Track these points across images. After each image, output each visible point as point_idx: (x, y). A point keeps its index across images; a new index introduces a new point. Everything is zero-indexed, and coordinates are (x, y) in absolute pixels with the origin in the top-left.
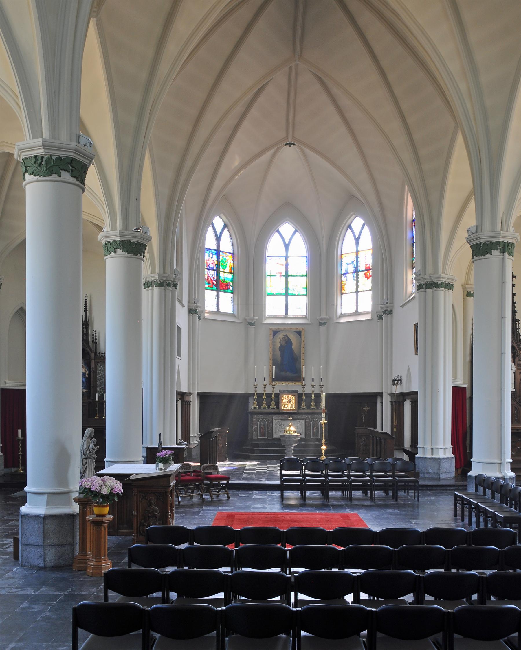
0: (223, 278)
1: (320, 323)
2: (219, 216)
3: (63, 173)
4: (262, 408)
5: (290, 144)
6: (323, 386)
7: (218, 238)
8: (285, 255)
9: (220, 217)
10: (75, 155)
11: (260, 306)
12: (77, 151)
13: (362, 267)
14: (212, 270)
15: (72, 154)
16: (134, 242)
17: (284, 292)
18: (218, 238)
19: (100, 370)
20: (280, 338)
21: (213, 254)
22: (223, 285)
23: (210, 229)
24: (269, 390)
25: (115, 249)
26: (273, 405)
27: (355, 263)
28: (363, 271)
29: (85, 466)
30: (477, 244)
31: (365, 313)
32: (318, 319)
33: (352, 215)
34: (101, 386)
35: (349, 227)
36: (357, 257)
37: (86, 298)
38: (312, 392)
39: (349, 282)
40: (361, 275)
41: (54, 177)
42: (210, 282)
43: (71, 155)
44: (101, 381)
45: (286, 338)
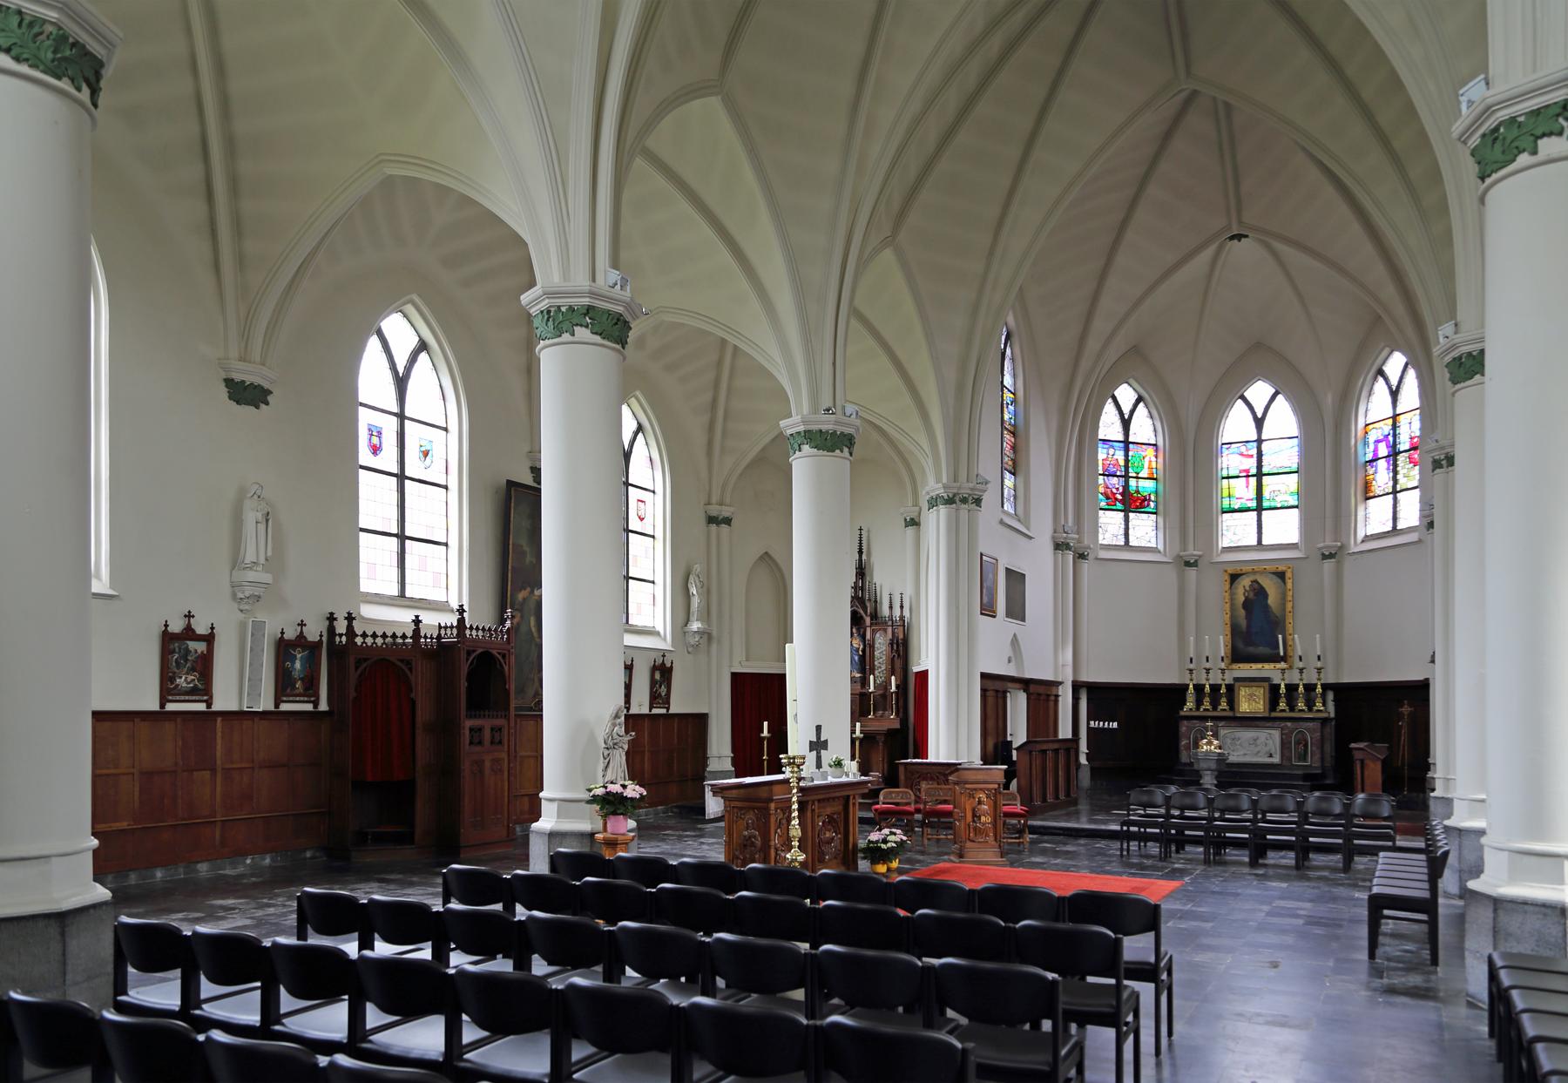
0: (1135, 488)
1: (1323, 554)
2: (1127, 383)
3: (577, 329)
4: (1202, 710)
5: (1239, 237)
7: (1126, 424)
8: (1255, 438)
9: (1129, 384)
10: (592, 301)
11: (1210, 530)
12: (592, 294)
13: (1404, 444)
14: (1114, 475)
15: (588, 299)
16: (827, 432)
17: (1253, 504)
18: (1126, 424)
19: (880, 643)
20: (1244, 587)
24: (1216, 678)
25: (799, 446)
26: (1224, 705)
27: (1391, 438)
28: (1405, 451)
29: (607, 760)
30: (1454, 359)
31: (1410, 530)
32: (1319, 549)
33: (1382, 350)
34: (880, 667)
35: (1381, 373)
36: (1394, 427)
38: (1297, 682)
39: (1381, 477)
40: (1401, 458)
41: (566, 337)
43: (586, 301)
45: (1256, 586)
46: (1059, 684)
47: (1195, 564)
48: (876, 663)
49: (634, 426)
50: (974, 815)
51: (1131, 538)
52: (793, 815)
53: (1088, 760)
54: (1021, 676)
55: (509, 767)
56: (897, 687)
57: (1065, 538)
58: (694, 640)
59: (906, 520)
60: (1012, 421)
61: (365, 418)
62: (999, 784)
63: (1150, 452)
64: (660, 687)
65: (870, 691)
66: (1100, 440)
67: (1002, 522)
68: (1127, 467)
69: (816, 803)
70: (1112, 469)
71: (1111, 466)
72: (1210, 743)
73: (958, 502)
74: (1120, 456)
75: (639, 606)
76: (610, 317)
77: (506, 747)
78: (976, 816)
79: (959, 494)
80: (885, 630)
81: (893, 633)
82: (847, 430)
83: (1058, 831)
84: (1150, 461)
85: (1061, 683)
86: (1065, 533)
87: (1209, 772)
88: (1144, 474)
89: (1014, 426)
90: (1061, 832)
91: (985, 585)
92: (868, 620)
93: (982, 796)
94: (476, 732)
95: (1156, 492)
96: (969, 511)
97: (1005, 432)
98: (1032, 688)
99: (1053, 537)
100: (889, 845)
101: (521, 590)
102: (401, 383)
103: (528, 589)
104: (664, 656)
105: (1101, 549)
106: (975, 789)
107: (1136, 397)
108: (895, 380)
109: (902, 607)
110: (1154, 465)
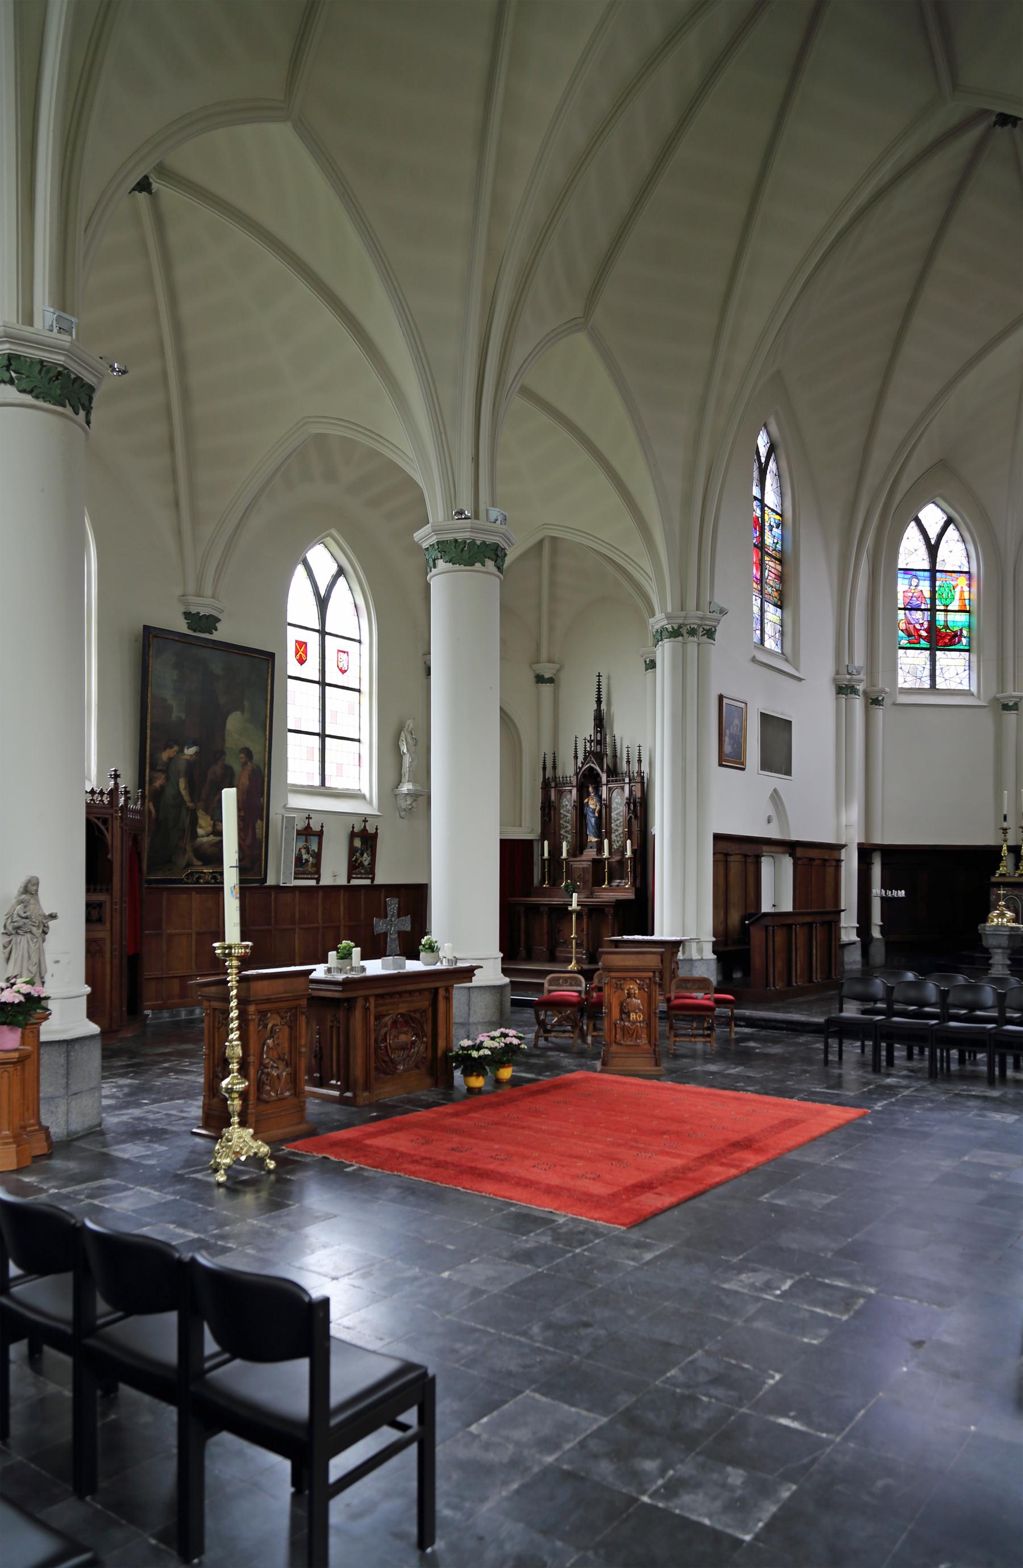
0: (942, 623)
2: (933, 503)
4: (997, 875)
6: (1008, 831)
7: (933, 550)
18: (933, 550)
19: (617, 803)
21: (919, 580)
22: (943, 636)
23: (912, 530)
25: (434, 560)
29: (8, 949)
37: (599, 679)
42: (912, 634)
44: (618, 822)
46: (841, 847)
47: (1015, 707)
48: (613, 825)
49: (334, 568)
50: (622, 1011)
51: (938, 680)
52: (231, 1026)
53: (882, 933)
54: (786, 838)
55: (111, 948)
56: (634, 852)
57: (849, 680)
58: (405, 804)
59: (645, 662)
60: (779, 547)
61: (293, 635)
62: (654, 972)
63: (962, 581)
64: (362, 855)
65: (604, 857)
66: (900, 569)
67: (754, 660)
68: (933, 599)
69: (372, 1000)
70: (915, 602)
71: (914, 599)
72: (1002, 915)
73: (685, 634)
74: (925, 587)
75: (340, 767)
76: (44, 369)
77: (108, 925)
78: (624, 1012)
79: (686, 625)
80: (623, 788)
81: (631, 791)
82: (491, 539)
83: (779, 1025)
84: (962, 592)
85: (843, 846)
86: (850, 674)
87: (1000, 951)
88: (955, 606)
89: (782, 552)
90: (784, 1026)
91: (727, 732)
92: (604, 778)
93: (634, 987)
94: (94, 908)
95: (969, 627)
96: (699, 644)
97: (767, 558)
98: (800, 853)
99: (835, 680)
100: (482, 1052)
101: (165, 749)
102: (322, 603)
103: (176, 748)
104: (365, 821)
105: (900, 693)
106: (624, 979)
107: (945, 519)
108: (615, 499)
109: (640, 761)
110: (966, 596)
